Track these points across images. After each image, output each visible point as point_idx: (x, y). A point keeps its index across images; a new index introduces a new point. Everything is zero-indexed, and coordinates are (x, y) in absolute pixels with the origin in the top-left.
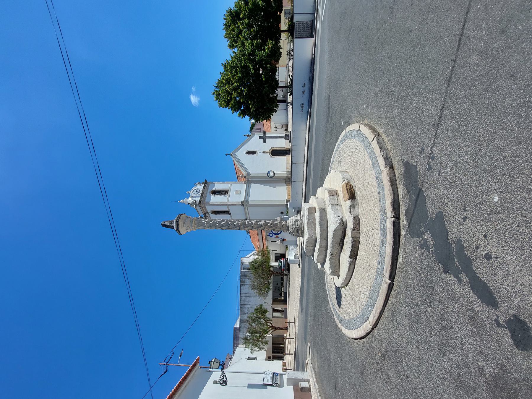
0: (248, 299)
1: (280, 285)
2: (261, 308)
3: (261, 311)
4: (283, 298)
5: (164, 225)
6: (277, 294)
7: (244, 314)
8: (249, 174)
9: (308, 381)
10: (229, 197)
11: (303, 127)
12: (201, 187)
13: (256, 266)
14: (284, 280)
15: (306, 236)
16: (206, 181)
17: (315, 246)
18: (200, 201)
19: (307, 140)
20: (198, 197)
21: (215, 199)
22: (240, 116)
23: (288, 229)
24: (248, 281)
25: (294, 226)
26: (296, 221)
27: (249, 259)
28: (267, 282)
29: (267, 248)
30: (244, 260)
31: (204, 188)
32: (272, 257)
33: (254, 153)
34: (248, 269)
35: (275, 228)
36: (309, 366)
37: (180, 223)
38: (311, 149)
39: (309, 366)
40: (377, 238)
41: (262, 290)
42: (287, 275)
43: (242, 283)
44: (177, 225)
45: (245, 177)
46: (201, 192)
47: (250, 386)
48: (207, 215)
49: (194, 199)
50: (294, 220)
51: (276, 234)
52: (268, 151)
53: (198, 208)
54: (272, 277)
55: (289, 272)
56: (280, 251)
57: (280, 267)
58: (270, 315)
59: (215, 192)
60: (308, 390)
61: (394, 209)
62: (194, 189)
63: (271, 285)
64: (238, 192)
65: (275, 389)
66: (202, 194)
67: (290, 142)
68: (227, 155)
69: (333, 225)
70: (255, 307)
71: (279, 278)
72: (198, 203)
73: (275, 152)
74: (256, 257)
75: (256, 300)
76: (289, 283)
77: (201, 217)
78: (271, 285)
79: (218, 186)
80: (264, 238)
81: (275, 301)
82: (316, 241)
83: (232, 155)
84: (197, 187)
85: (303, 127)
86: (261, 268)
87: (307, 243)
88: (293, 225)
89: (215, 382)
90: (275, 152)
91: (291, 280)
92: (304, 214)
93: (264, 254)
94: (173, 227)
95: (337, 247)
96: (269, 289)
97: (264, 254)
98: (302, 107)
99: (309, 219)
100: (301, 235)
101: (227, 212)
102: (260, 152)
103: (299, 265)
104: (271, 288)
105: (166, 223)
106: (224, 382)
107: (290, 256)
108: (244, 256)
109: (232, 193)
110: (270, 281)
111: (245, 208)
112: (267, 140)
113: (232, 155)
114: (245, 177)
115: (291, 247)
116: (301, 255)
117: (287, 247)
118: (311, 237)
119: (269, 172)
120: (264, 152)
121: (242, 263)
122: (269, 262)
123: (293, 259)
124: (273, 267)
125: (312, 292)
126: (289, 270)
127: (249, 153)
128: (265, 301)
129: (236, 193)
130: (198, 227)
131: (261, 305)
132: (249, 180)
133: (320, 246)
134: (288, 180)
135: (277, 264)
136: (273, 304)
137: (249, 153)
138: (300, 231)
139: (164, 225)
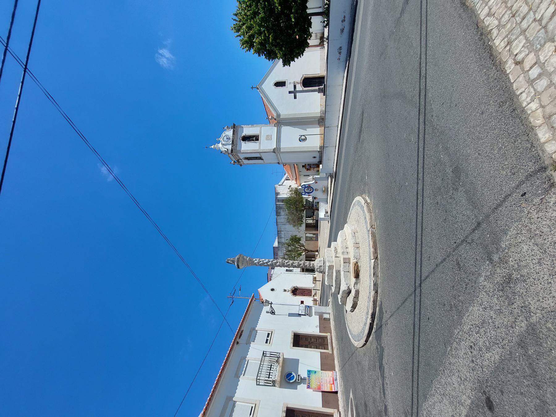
3: (296, 240)
7: (281, 238)
8: (278, 115)
9: (329, 314)
10: (260, 143)
12: (230, 133)
16: (234, 125)
18: (232, 150)
19: (336, 159)
20: (229, 144)
21: (247, 147)
27: (284, 192)
31: (233, 134)
36: (330, 304)
37: (240, 265)
38: (348, 105)
39: (330, 304)
40: (366, 298)
43: (278, 214)
45: (275, 119)
46: (231, 138)
47: (290, 315)
48: (240, 161)
49: (225, 147)
53: (231, 155)
58: (303, 241)
59: (246, 138)
60: (329, 319)
61: (372, 317)
62: (224, 135)
64: (269, 138)
65: (307, 317)
66: (233, 141)
68: (252, 88)
69: (343, 287)
72: (230, 152)
73: (295, 291)
75: (290, 230)
79: (248, 131)
89: (267, 312)
90: (295, 291)
95: (345, 295)
98: (340, 53)
101: (260, 158)
106: (273, 313)
109: (262, 138)
112: (298, 95)
113: (258, 89)
114: (275, 119)
121: (277, 194)
123: (323, 217)
129: (267, 139)
134: (321, 121)
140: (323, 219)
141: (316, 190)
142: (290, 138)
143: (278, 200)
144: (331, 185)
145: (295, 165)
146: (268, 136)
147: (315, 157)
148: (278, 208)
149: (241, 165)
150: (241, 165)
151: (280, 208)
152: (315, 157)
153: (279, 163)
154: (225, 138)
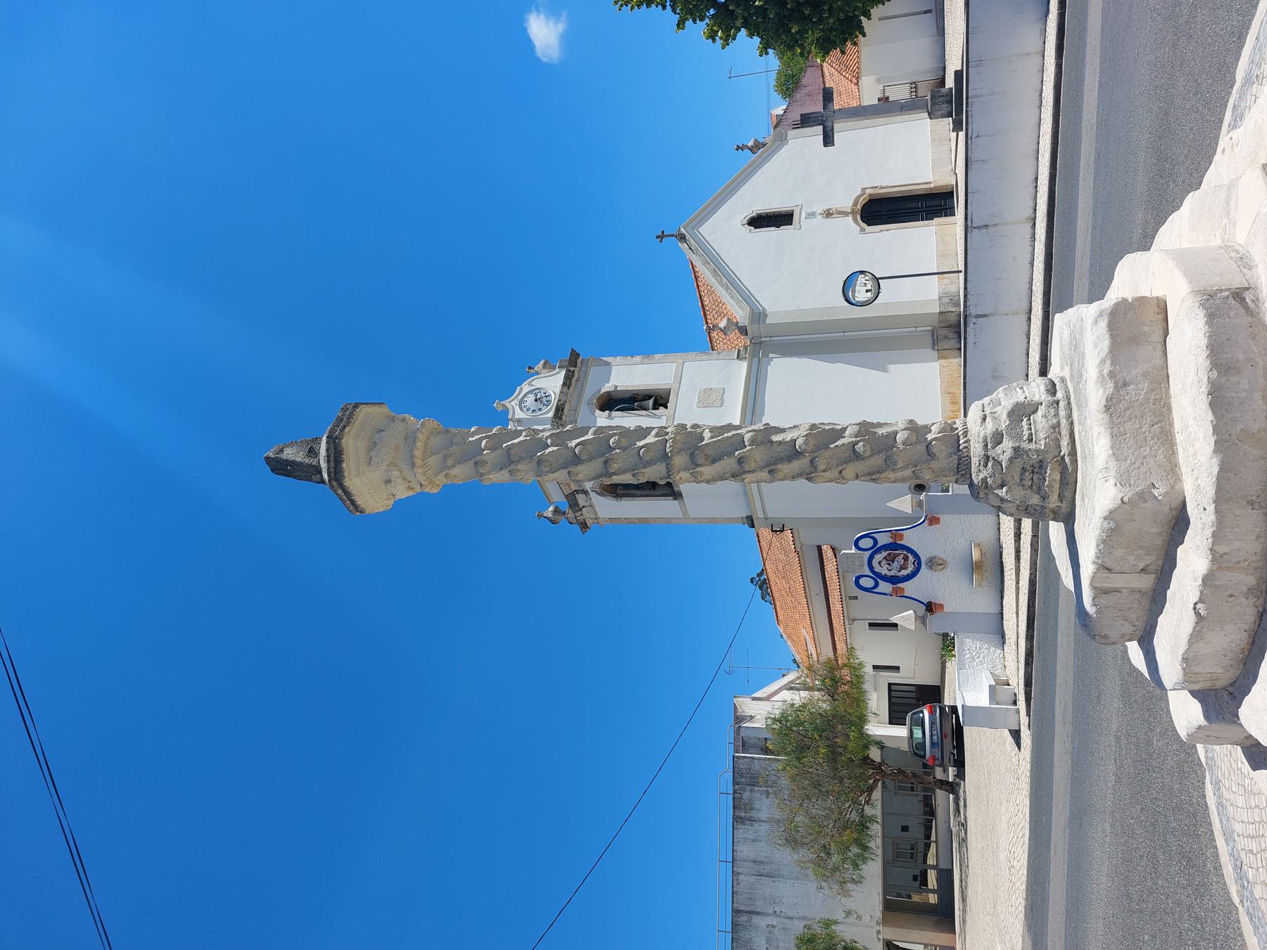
0: (767, 888)
1: (917, 832)
2: (831, 936)
4: (933, 899)
5: (280, 467)
6: (905, 874)
8: (758, 316)
11: (1029, 39)
12: (552, 383)
13: (794, 734)
14: (940, 811)
15: (1098, 495)
16: (575, 355)
17: (1168, 565)
22: (712, 36)
23: (962, 469)
24: (765, 807)
25: (1007, 445)
26: (1022, 412)
27: (765, 706)
28: (854, 816)
29: (851, 651)
30: (748, 706)
31: (567, 383)
32: (877, 701)
33: (781, 219)
34: (766, 751)
35: (878, 461)
37: (352, 444)
41: (834, 850)
42: (952, 788)
43: (741, 814)
44: (336, 456)
45: (743, 331)
48: (581, 499)
50: (1002, 413)
51: (893, 580)
52: (847, 203)
54: (877, 795)
55: (961, 774)
56: (915, 672)
57: (917, 749)
63: (876, 829)
66: (559, 410)
67: (957, 127)
68: (661, 237)
70: (798, 927)
71: (913, 804)
73: (882, 210)
74: (798, 698)
76: (964, 825)
77: (556, 511)
78: (876, 829)
79: (627, 375)
80: (836, 607)
81: (897, 907)
82: (1179, 523)
83: (682, 238)
84: (539, 383)
85: (1029, 39)
86: (824, 744)
87: (1108, 541)
88: (998, 438)
90: (882, 210)
91: (974, 813)
92: (1078, 376)
93: (836, 682)
94: (318, 470)
96: (865, 848)
97: (839, 681)
99: (1119, 382)
100: (1053, 502)
102: (811, 215)
103: (1016, 735)
104: (876, 844)
105: (289, 454)
107: (969, 688)
108: (748, 689)
110: (868, 811)
111: (746, 494)
113: (682, 238)
114: (743, 331)
115: (969, 646)
116: (1028, 684)
117: (947, 644)
118: (1144, 496)
119: (848, 284)
120: (828, 214)
121: (739, 719)
122: (862, 720)
124: (880, 745)
125: (1101, 882)
126: (960, 764)
127: (759, 221)
128: (849, 903)
129: (705, 391)
130: (444, 467)
131: (828, 924)
132: (763, 341)
133: (1217, 558)
135: (901, 731)
136: (885, 921)
137: (759, 221)
138: (1052, 474)
139: (280, 467)
140: (984, 717)
141: (934, 563)
142: (806, 397)
143: (744, 744)
144: (1018, 536)
145: (828, 553)
146: (708, 392)
147: (905, 829)
148: (744, 780)
149: (584, 526)
150: (584, 526)
151: (753, 781)
152: (905, 829)
153: (751, 522)
154: (531, 398)
